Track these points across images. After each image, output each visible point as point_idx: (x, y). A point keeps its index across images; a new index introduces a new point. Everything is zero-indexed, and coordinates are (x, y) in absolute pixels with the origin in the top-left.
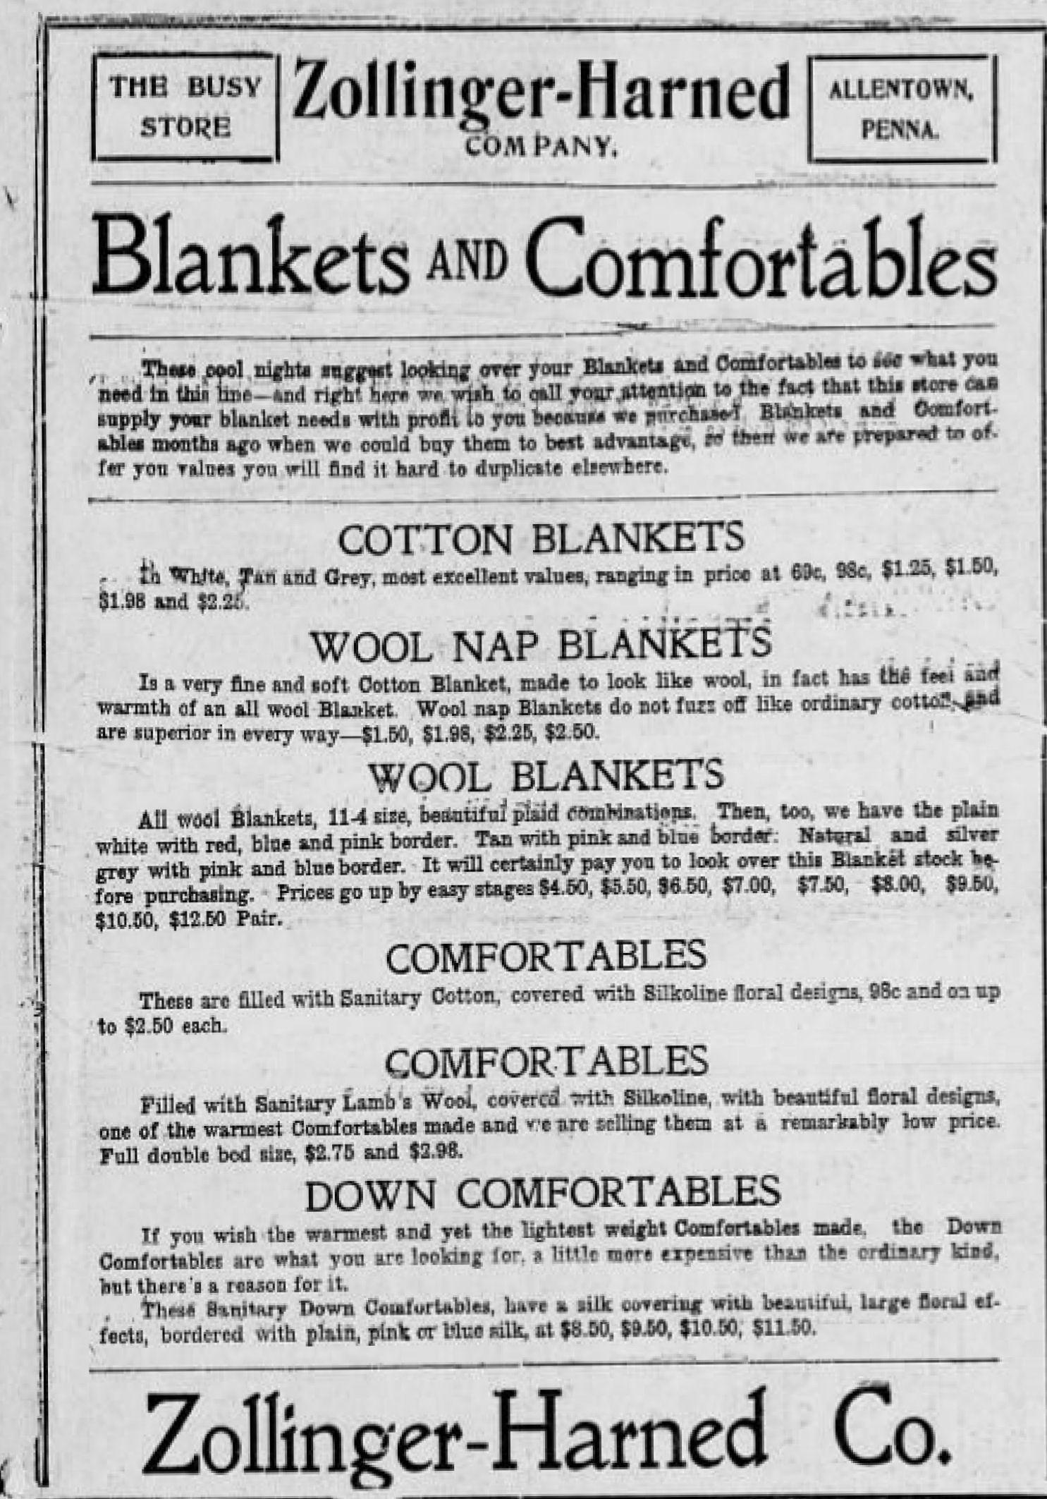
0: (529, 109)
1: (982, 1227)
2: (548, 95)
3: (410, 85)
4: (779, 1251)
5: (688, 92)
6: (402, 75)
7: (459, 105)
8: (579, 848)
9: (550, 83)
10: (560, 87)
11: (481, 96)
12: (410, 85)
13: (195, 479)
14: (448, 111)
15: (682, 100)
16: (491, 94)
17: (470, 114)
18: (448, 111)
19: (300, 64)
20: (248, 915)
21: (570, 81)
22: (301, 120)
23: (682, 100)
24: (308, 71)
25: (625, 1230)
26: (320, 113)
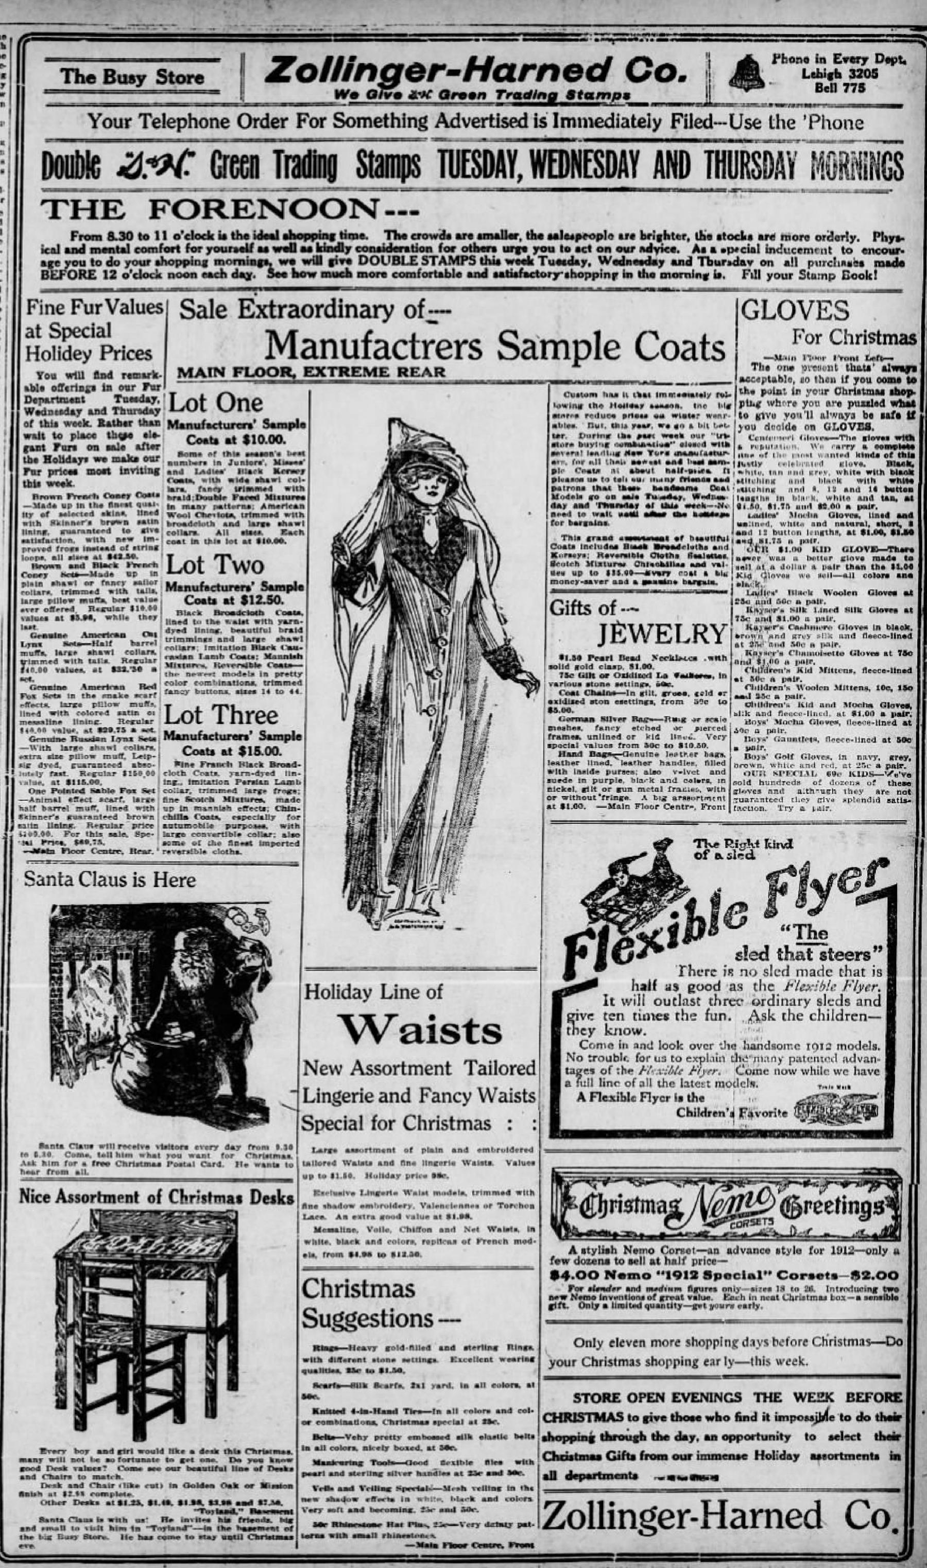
2: (687, 1518)
3: (612, 1513)
6: (607, 1508)
12: (612, 1513)
15: (761, 1519)
26: (561, 1527)
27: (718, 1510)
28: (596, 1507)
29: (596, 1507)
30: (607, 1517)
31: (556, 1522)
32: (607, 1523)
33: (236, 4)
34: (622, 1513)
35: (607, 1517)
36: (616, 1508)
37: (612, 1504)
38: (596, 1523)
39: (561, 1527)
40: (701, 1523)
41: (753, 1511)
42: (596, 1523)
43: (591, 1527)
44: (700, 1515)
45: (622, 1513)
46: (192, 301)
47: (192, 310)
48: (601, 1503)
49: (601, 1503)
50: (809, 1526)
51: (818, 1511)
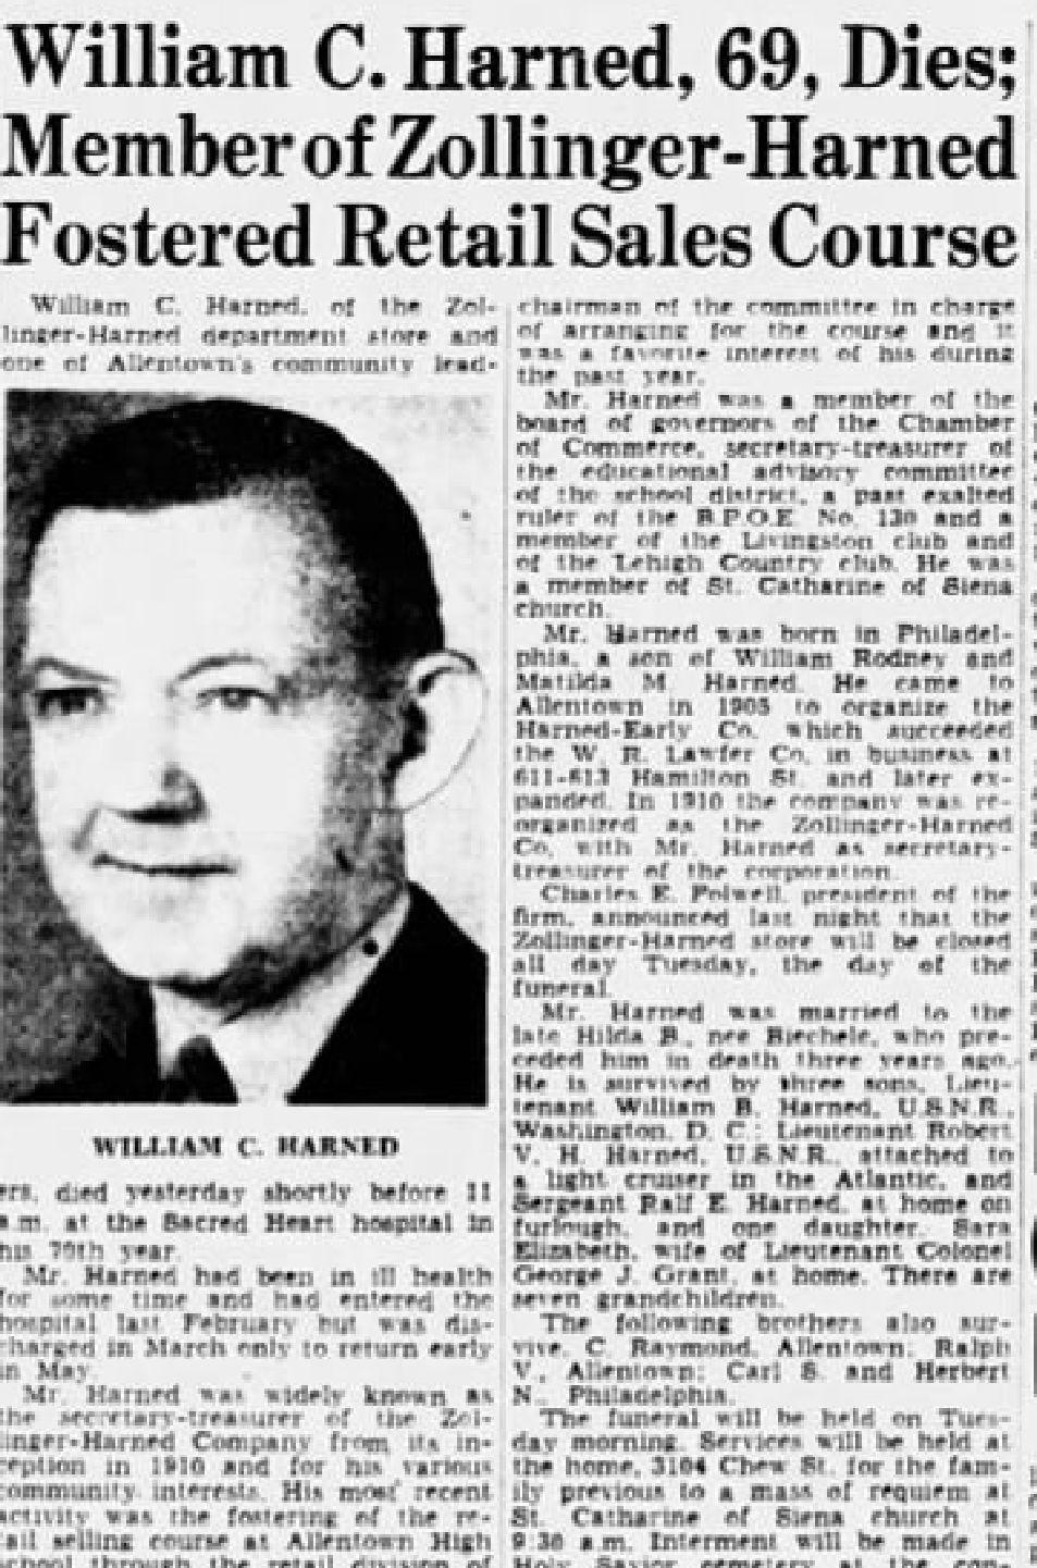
0: (113, 167)
1: (810, 634)
2: (713, 158)
3: (540, 142)
4: (988, 962)
5: (891, 150)
6: (528, 130)
7: (600, 162)
8: (276, 215)
9: (714, 142)
10: (727, 147)
11: (630, 156)
12: (540, 142)
13: (450, 1361)
14: (588, 171)
15: (883, 160)
16: (644, 154)
17: (613, 171)
18: (588, 171)
19: (398, 120)
20: (582, 1392)
21: (744, 140)
22: (398, 182)
23: (883, 160)
24: (407, 128)
25: (224, 155)
26: (427, 172)
27: (440, 51)
28: (503, 132)
29: (503, 132)
30: (160, 60)
31: (416, 163)
32: (528, 163)
33: (285, 1564)
34: (565, 142)
35: (160, 60)
36: (550, 132)
37: (540, 121)
38: (503, 162)
39: (427, 172)
40: (750, 163)
41: (209, 229)
42: (503, 162)
43: (490, 170)
44: (749, 149)
45: (565, 142)
46: (606, 213)
47: (605, 240)
48: (515, 121)
49: (515, 121)
50: (986, 173)
51: (1007, 143)
